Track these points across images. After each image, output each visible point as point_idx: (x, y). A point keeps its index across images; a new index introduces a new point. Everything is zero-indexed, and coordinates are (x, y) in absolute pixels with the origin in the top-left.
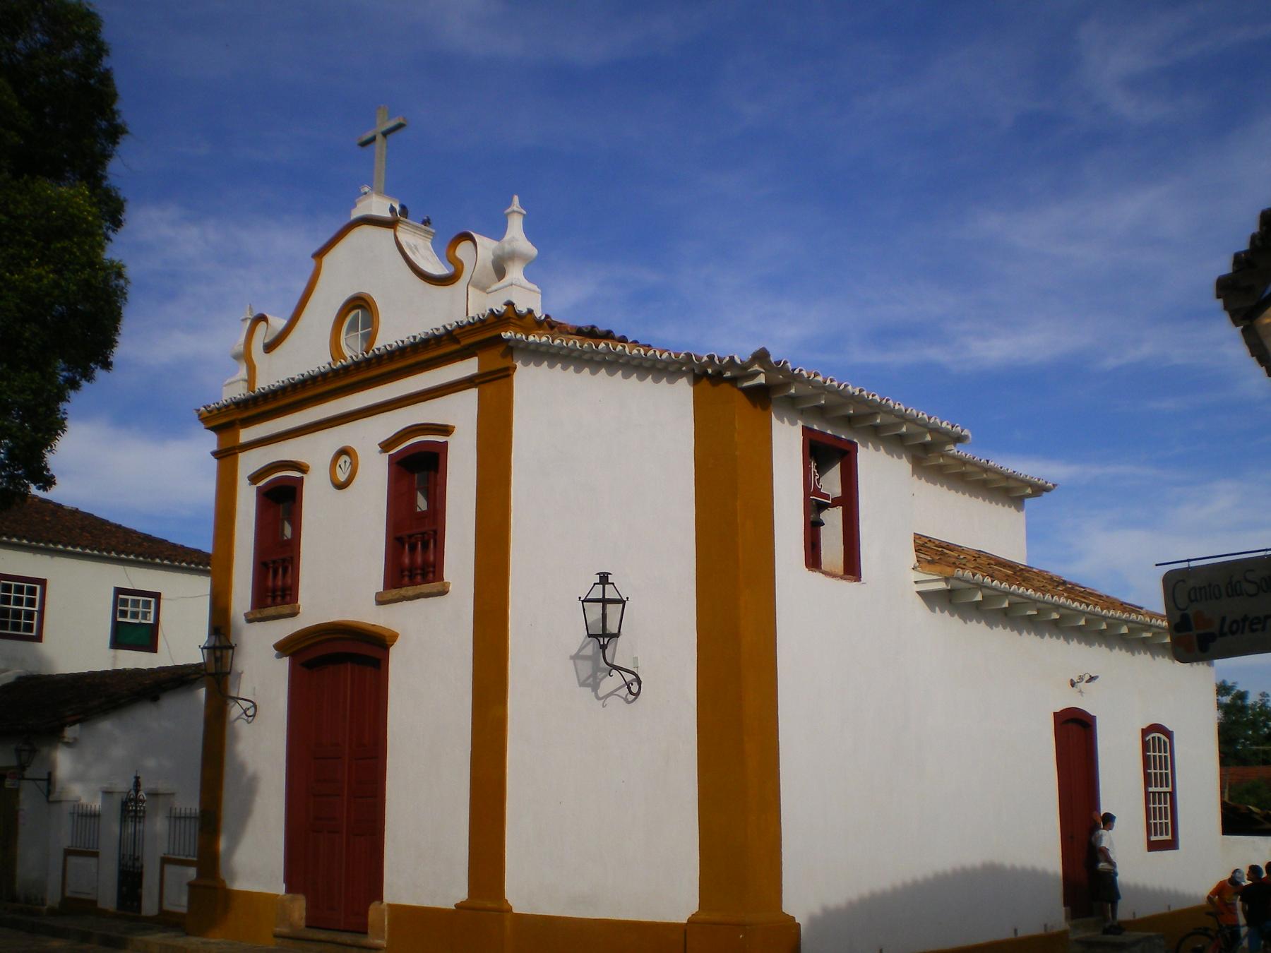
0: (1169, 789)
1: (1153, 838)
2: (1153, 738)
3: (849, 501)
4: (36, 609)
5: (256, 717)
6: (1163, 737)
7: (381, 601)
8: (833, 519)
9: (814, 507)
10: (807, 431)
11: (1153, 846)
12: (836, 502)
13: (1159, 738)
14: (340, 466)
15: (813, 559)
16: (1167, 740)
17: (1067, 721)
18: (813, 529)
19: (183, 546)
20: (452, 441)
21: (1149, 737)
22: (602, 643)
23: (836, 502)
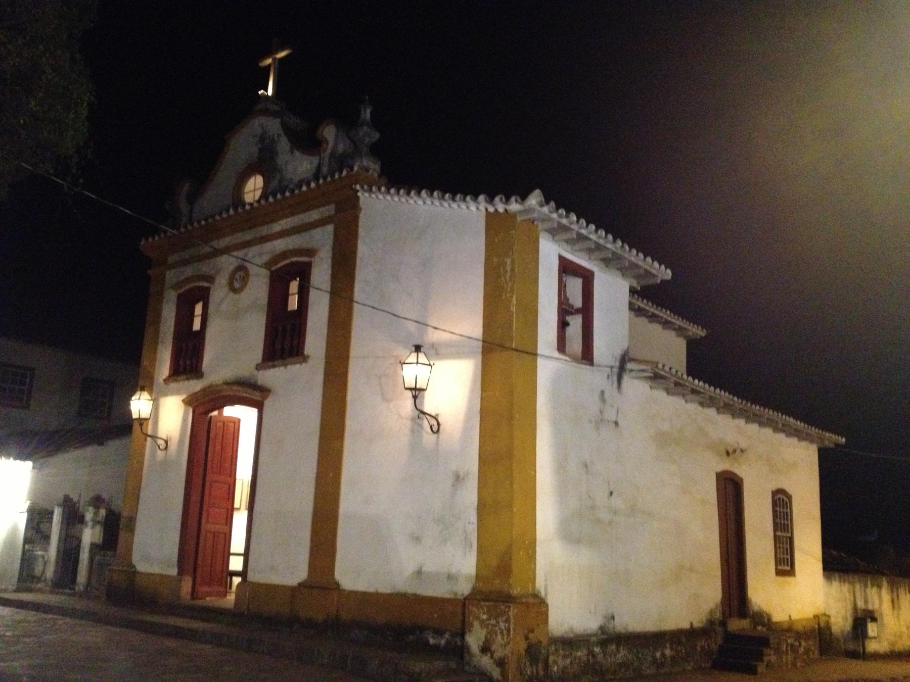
0: (789, 535)
1: (779, 567)
2: (779, 499)
3: (587, 311)
4: (27, 387)
5: (168, 448)
6: (785, 499)
7: (258, 367)
8: (575, 323)
9: (565, 310)
10: (562, 259)
11: (779, 573)
12: (578, 311)
13: (783, 500)
14: (236, 279)
15: (562, 345)
16: (788, 501)
17: (725, 479)
18: (563, 325)
19: (101, 443)
20: (316, 260)
21: (777, 497)
22: (414, 394)
23: (578, 311)
